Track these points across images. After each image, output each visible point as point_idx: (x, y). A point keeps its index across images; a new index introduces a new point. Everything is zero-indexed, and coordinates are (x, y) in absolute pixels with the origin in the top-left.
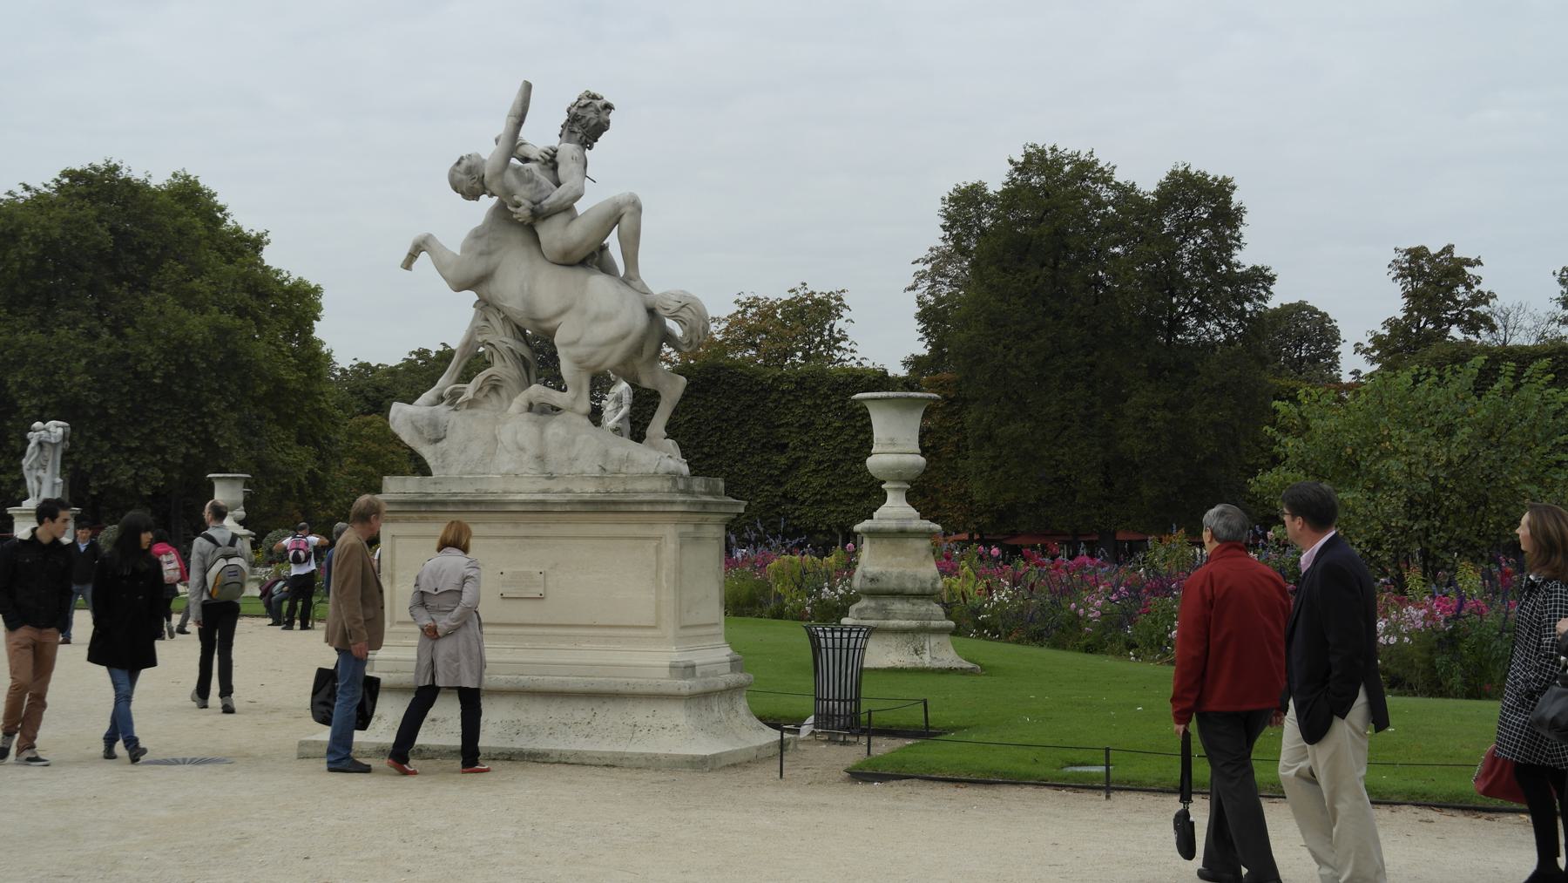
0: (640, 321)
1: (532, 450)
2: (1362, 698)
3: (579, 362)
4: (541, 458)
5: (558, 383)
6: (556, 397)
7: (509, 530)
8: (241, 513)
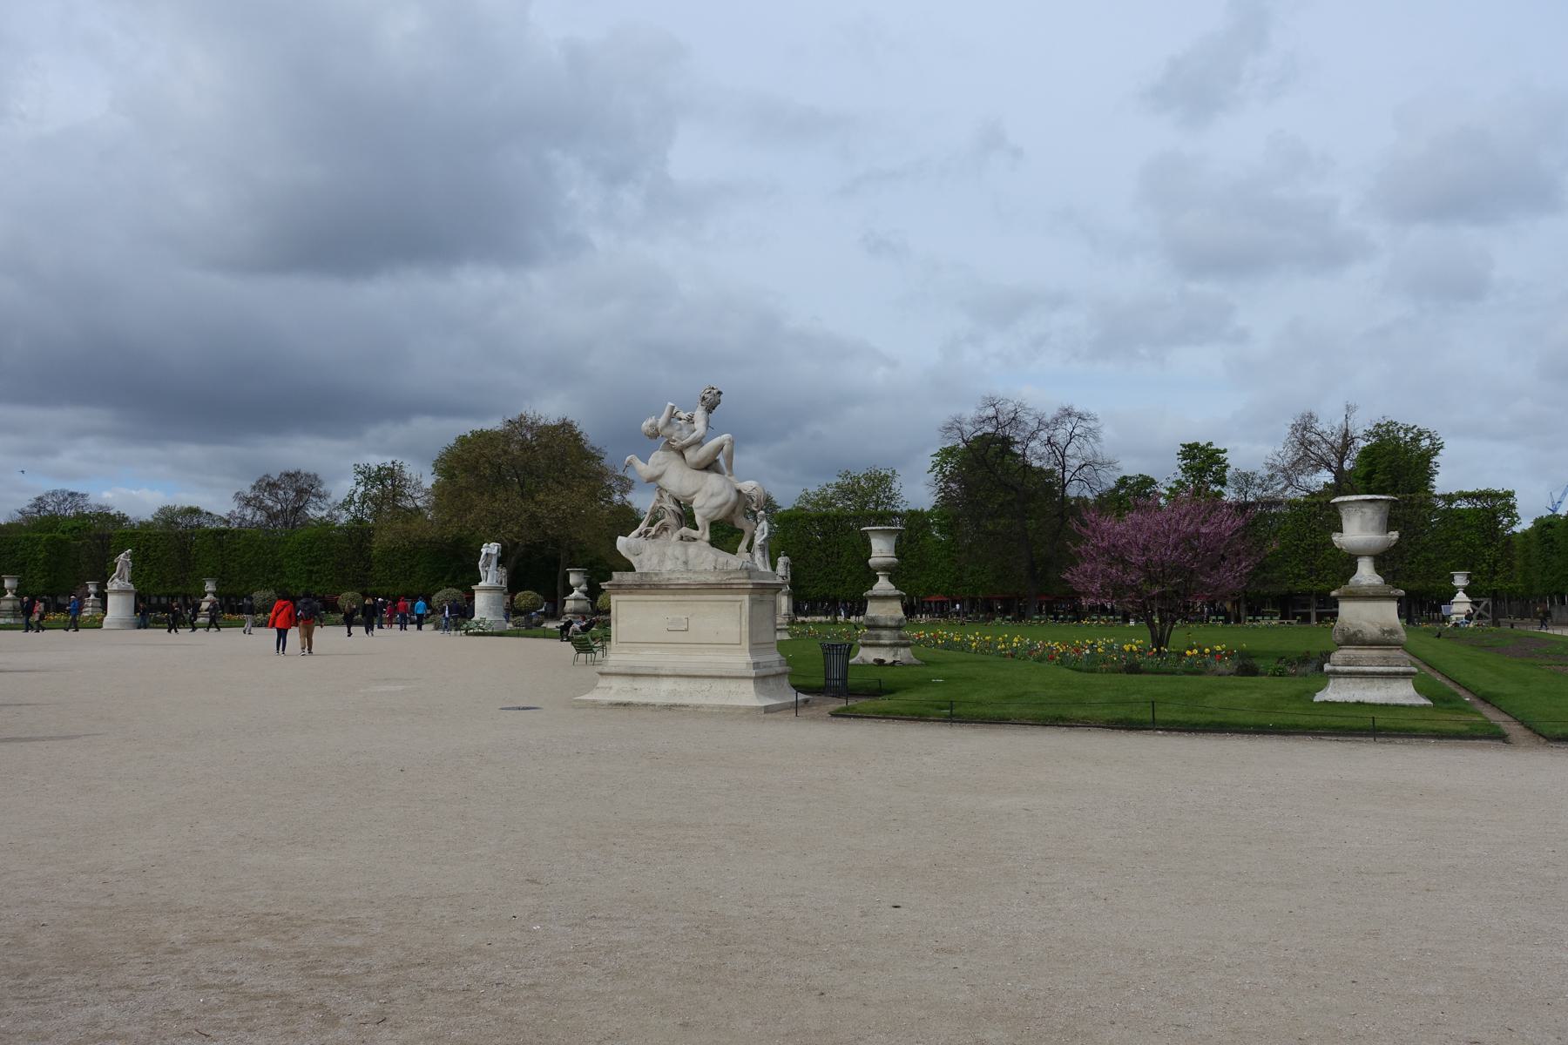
0: (733, 497)
1: (683, 559)
2: (1423, 701)
3: (704, 516)
4: (686, 563)
5: (696, 528)
6: (694, 533)
7: (671, 597)
8: (584, 587)
